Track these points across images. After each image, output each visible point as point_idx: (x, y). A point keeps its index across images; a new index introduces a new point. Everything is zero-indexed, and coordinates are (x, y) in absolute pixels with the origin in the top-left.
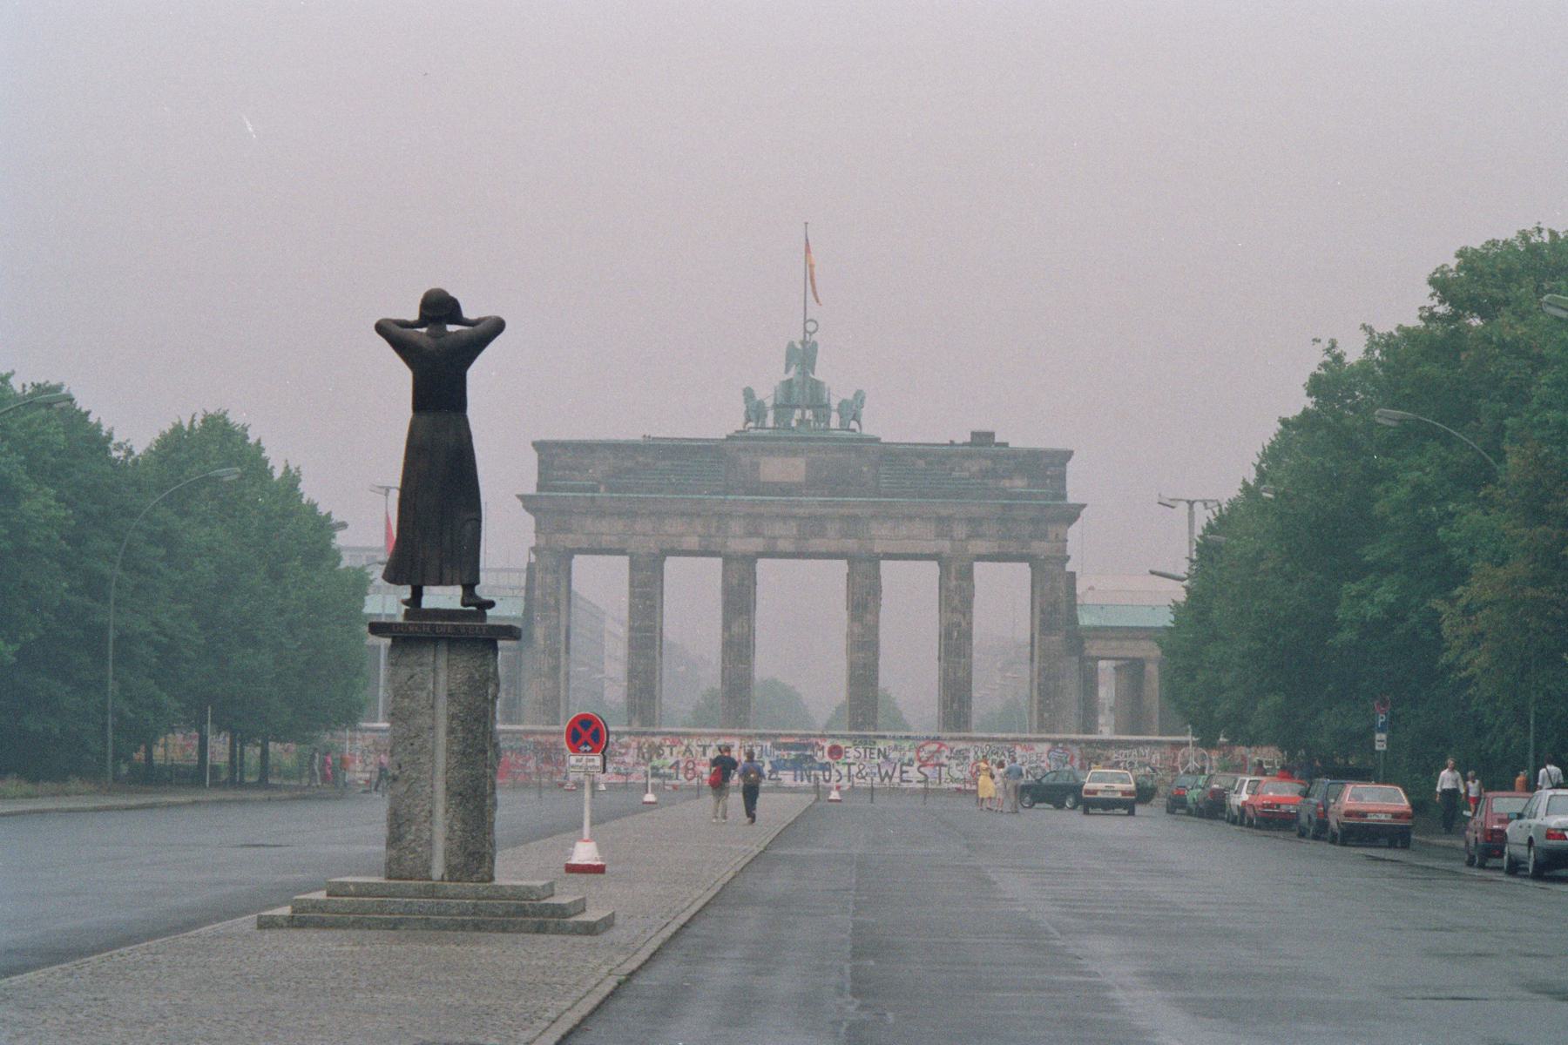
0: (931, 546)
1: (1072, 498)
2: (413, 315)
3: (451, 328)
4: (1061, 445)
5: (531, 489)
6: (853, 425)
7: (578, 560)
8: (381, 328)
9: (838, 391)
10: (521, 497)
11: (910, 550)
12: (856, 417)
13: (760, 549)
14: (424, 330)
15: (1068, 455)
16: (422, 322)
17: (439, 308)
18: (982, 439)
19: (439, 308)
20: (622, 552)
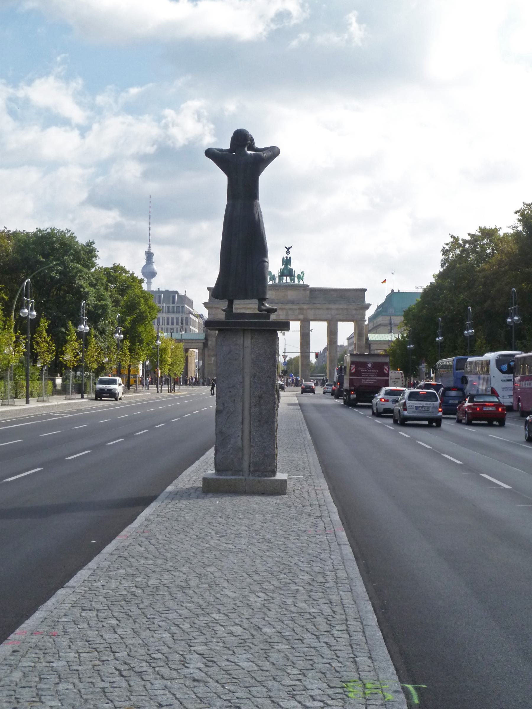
9: (297, 272)
10: (205, 304)
12: (302, 279)
15: (366, 290)
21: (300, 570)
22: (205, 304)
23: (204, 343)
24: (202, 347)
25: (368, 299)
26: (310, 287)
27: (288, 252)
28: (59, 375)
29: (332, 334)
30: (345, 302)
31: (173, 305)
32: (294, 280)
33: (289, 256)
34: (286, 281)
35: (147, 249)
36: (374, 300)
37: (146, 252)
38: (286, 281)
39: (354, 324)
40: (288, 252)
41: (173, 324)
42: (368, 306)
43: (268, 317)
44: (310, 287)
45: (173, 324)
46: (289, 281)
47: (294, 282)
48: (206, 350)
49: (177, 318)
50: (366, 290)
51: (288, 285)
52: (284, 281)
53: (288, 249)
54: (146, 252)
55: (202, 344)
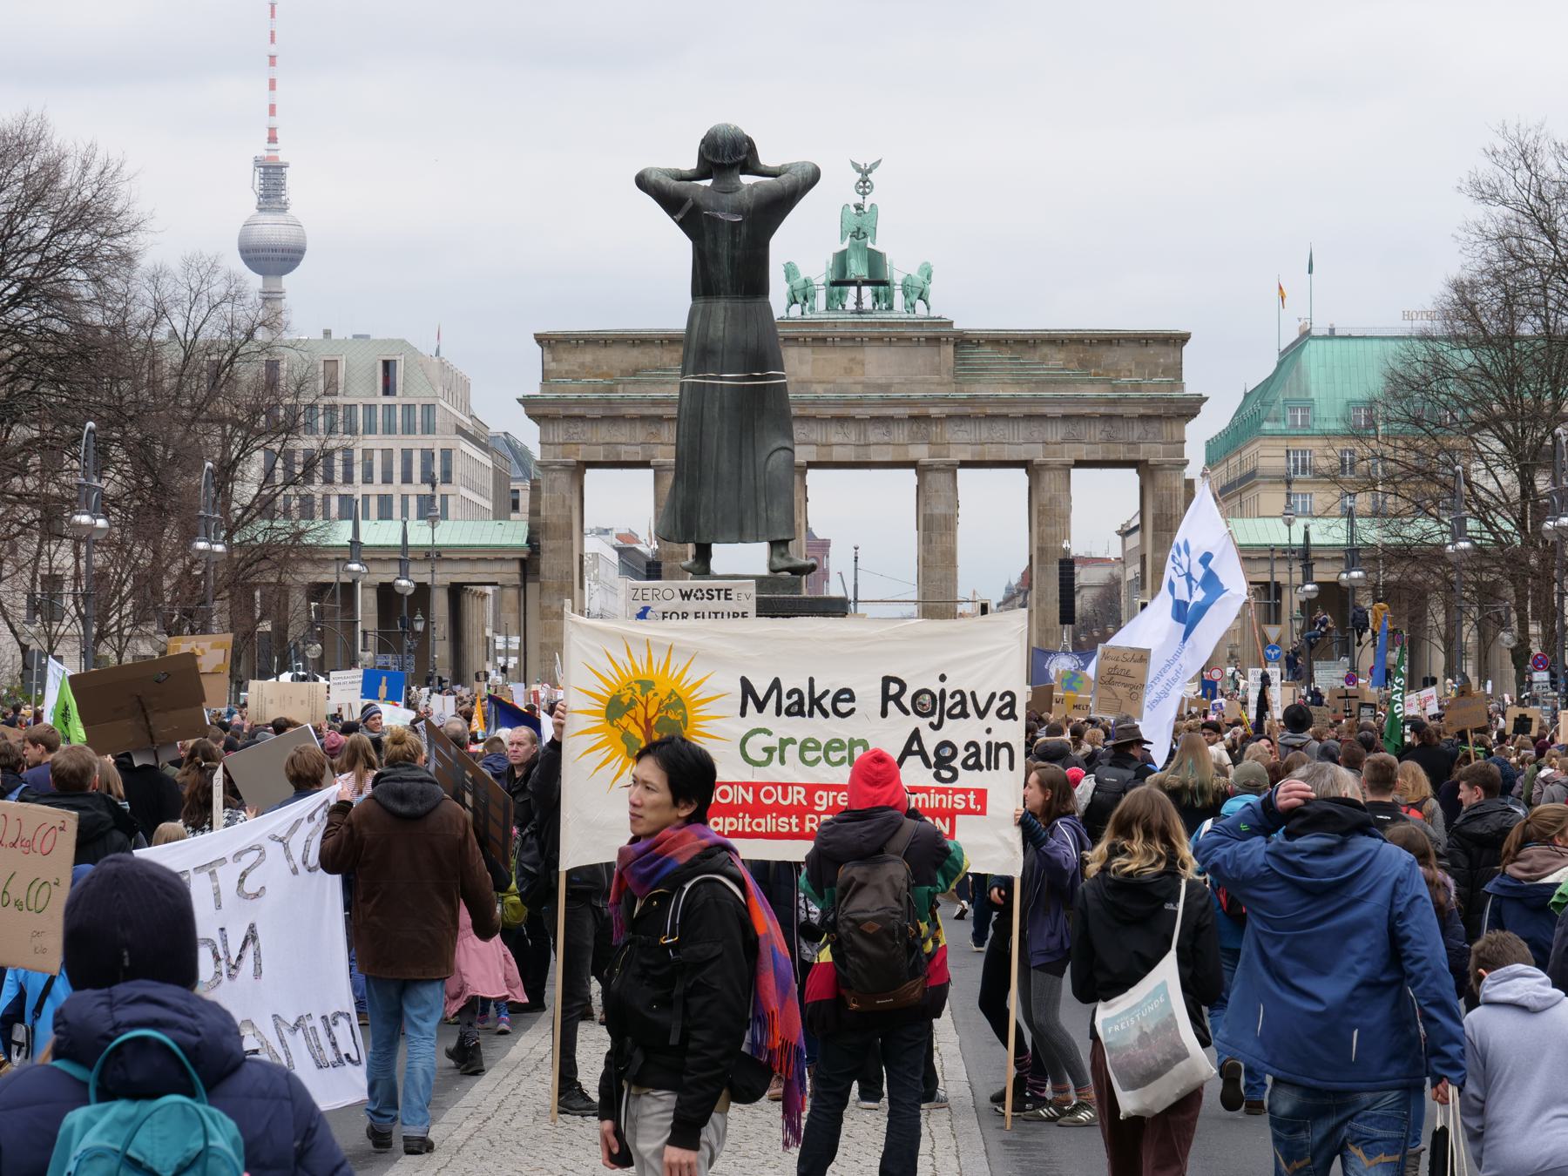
0: (1021, 453)
1: (1191, 386)
2: (690, 163)
3: (747, 180)
4: (1183, 329)
5: (534, 389)
6: (920, 305)
7: (591, 475)
8: (642, 182)
9: (899, 268)
10: (526, 402)
11: (1112, 457)
12: (922, 296)
13: (813, 458)
14: (708, 183)
15: (1183, 339)
16: (701, 174)
17: (727, 154)
18: (403, 341)
19: (727, 154)
20: (644, 464)
21: (770, 734)
22: (526, 402)
23: (523, 563)
24: (516, 579)
25: (1198, 372)
26: (956, 326)
27: (864, 185)
28: (776, 1089)
29: (1047, 514)
30: (1104, 394)
31: (388, 400)
32: (889, 297)
33: (869, 200)
34: (859, 302)
35: (261, 149)
36: (1219, 379)
37: (258, 163)
38: (859, 302)
39: (1137, 478)
40: (864, 185)
41: (387, 479)
42: (1190, 408)
43: (796, 587)
44: (956, 326)
45: (387, 479)
46: (867, 303)
47: (890, 308)
48: (532, 588)
49: (407, 455)
50: (1183, 339)
51: (866, 318)
52: (850, 303)
53: (865, 173)
54: (258, 163)
55: (516, 567)
